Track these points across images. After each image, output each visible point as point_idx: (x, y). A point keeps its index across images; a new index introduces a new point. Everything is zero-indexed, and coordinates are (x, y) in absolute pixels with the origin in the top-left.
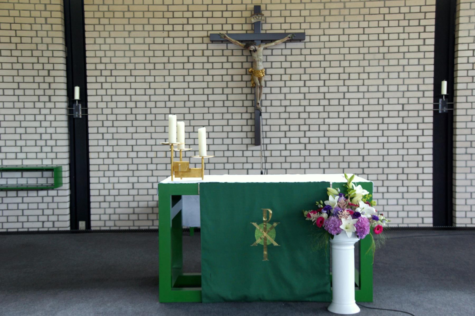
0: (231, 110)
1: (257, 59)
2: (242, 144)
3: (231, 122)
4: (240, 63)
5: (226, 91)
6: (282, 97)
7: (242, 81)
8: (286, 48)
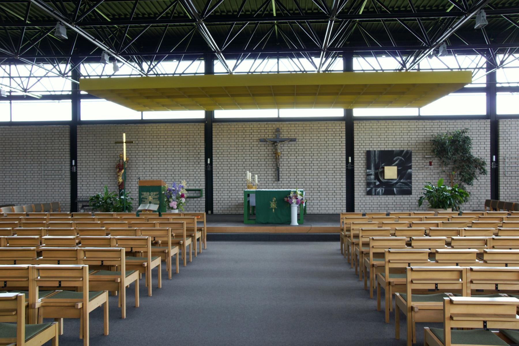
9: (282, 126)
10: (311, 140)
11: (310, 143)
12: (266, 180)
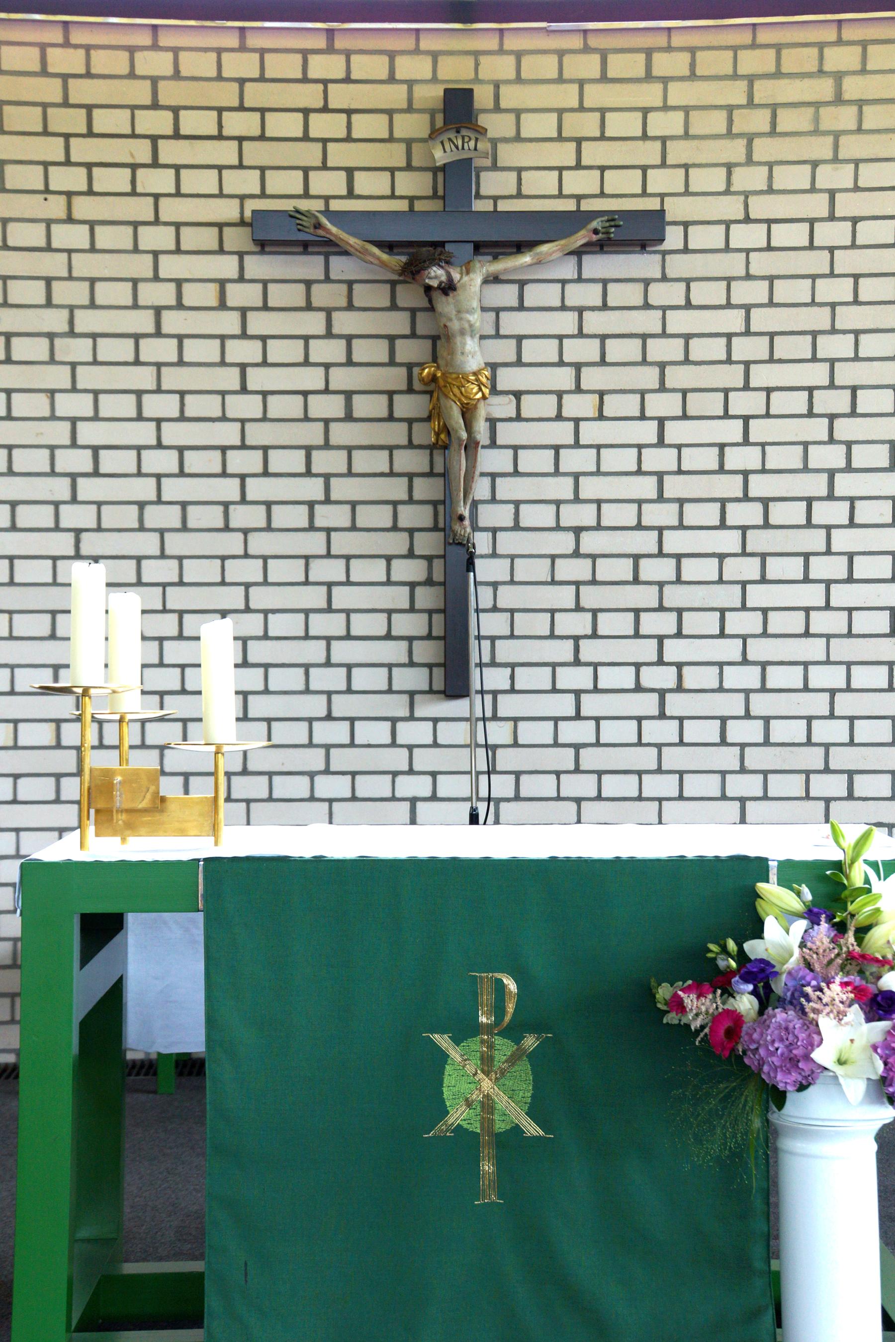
1: (455, 326)
2: (390, 691)
6: (562, 488)
8: (580, 280)
9: (504, 67)
10: (827, 234)
11: (818, 262)
12: (322, 679)
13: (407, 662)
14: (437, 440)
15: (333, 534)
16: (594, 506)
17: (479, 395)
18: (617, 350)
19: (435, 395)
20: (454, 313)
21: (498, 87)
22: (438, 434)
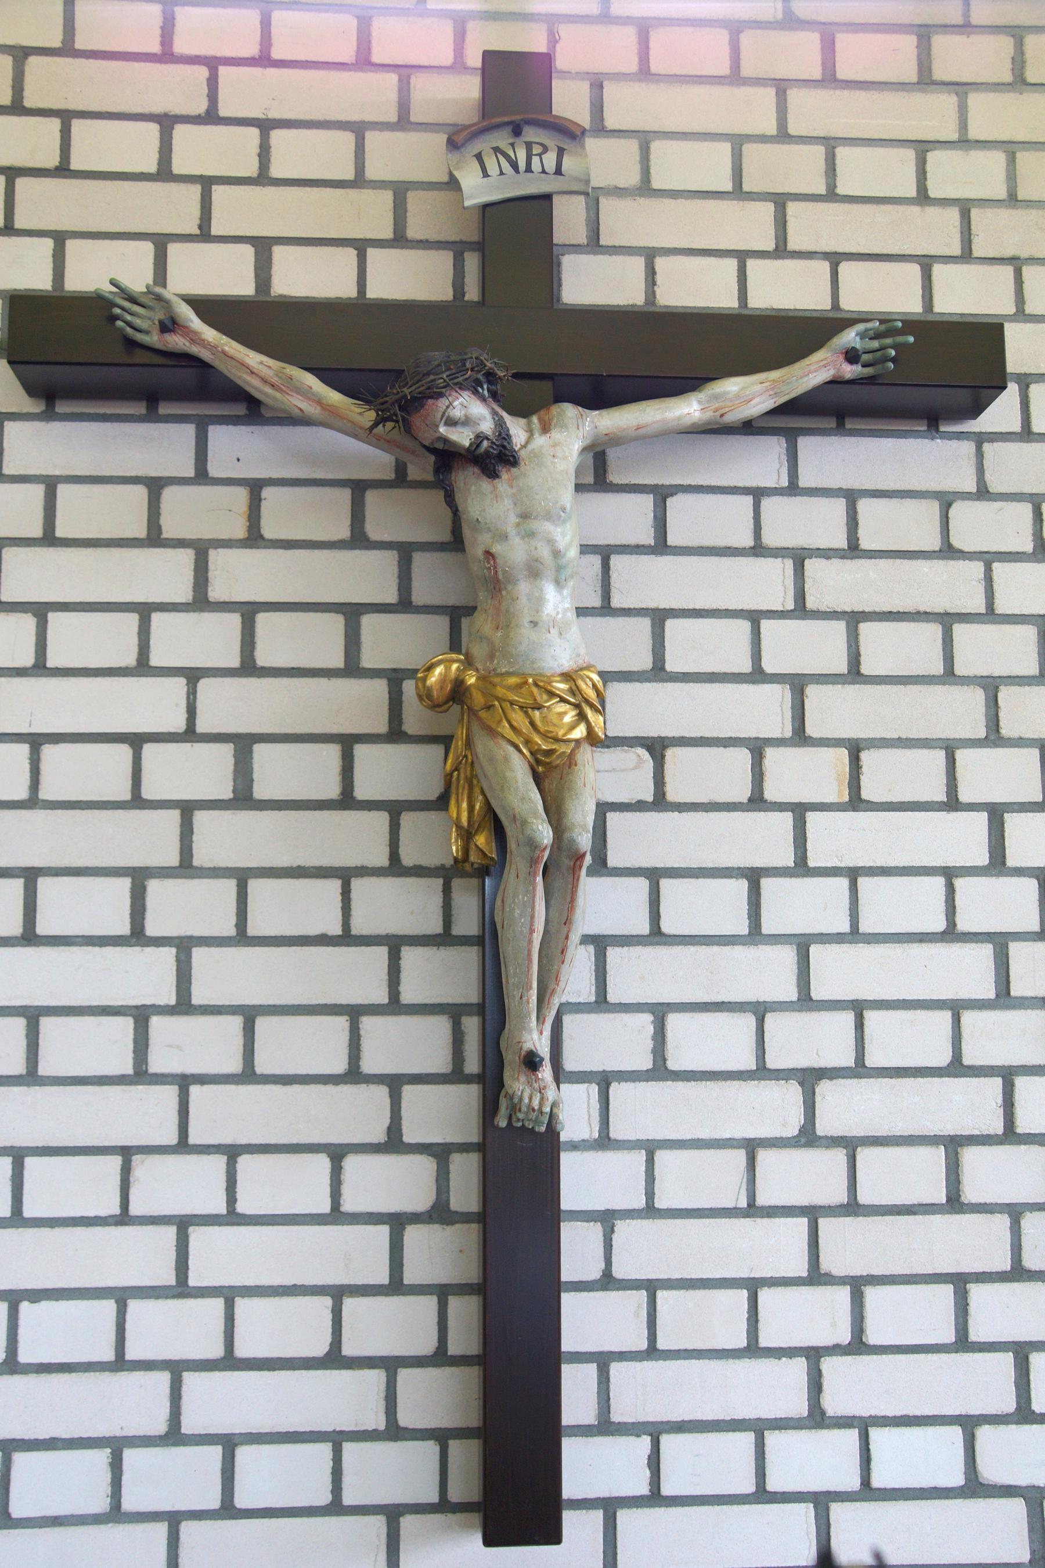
0: (217, 1114)
1: (514, 552)
2: (336, 1507)
3: (216, 1256)
4: (336, 623)
5: (173, 908)
6: (770, 974)
7: (346, 800)
8: (793, 489)
13: (382, 1426)
14: (466, 851)
15: (195, 1090)
16: (848, 1018)
17: (580, 732)
18: (884, 648)
19: (459, 744)
20: (513, 519)
21: (601, 86)
22: (467, 836)
